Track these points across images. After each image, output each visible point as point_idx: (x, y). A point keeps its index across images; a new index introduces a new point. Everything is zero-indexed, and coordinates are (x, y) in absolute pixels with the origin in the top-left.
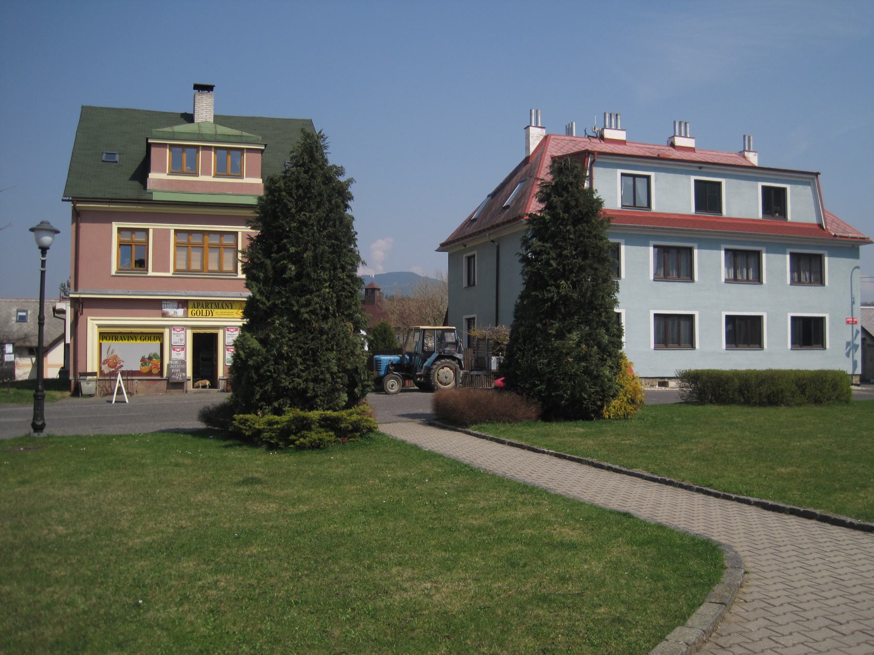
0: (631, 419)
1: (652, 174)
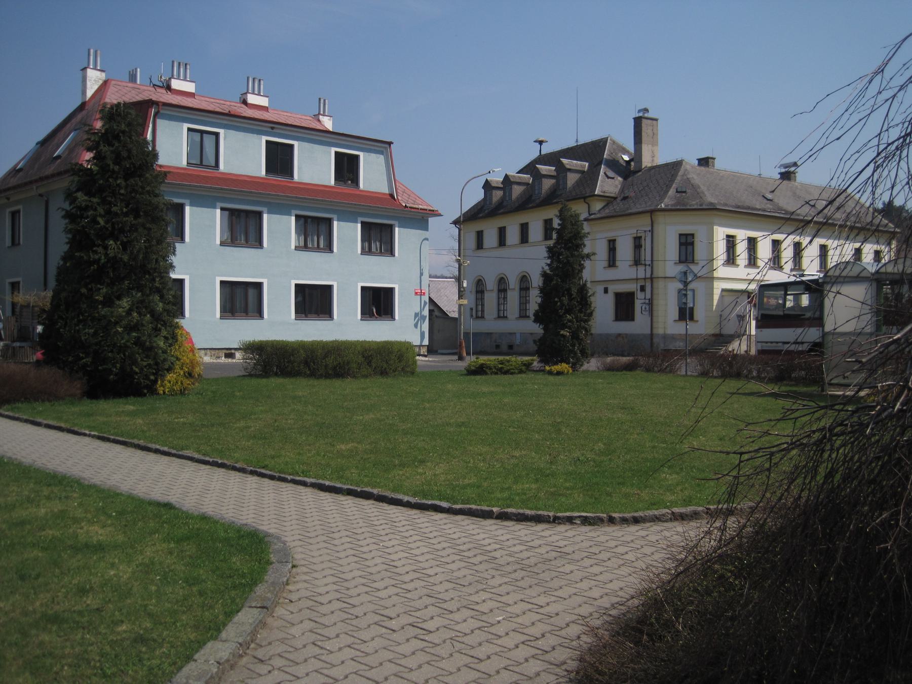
0: (189, 394)
1: (221, 131)
